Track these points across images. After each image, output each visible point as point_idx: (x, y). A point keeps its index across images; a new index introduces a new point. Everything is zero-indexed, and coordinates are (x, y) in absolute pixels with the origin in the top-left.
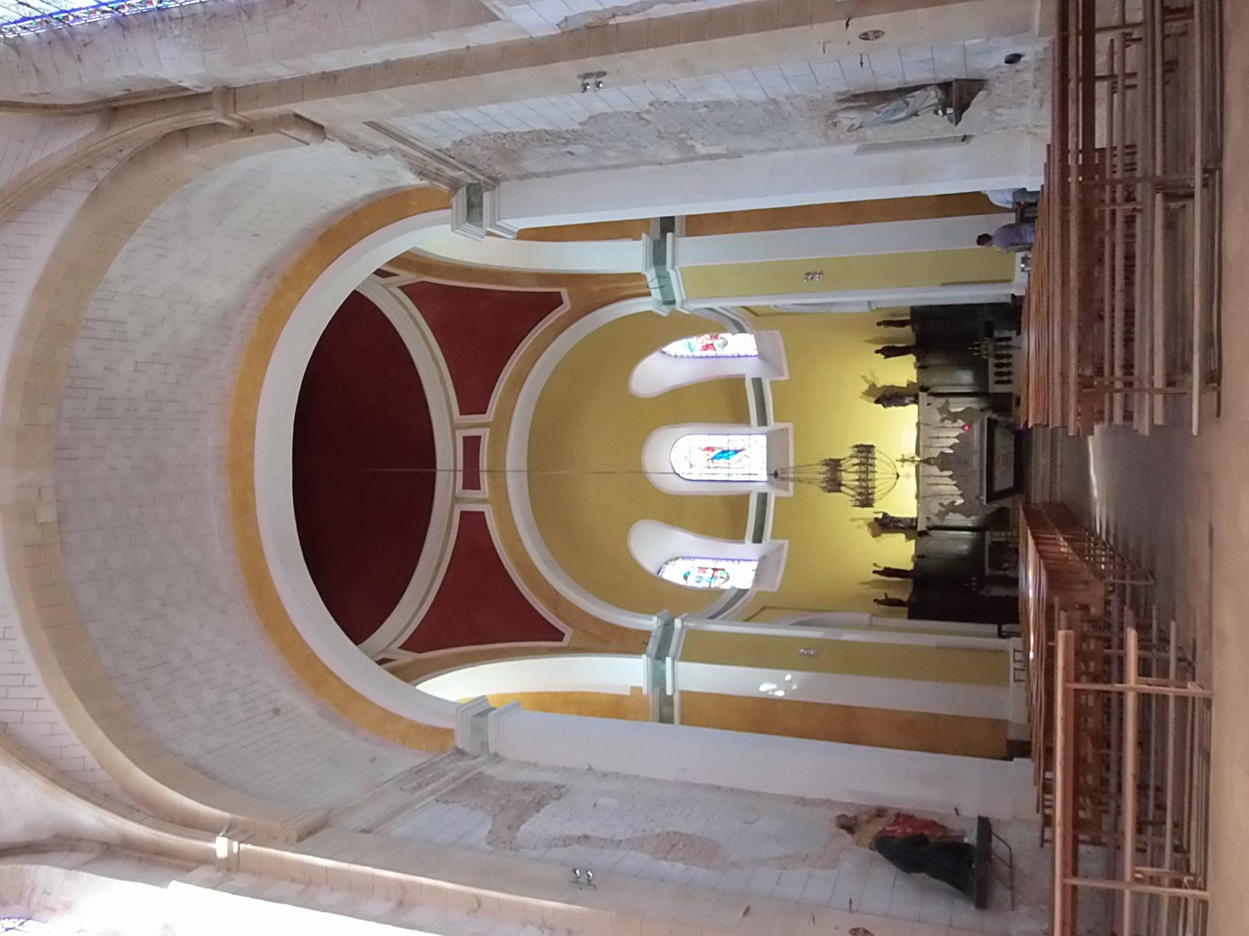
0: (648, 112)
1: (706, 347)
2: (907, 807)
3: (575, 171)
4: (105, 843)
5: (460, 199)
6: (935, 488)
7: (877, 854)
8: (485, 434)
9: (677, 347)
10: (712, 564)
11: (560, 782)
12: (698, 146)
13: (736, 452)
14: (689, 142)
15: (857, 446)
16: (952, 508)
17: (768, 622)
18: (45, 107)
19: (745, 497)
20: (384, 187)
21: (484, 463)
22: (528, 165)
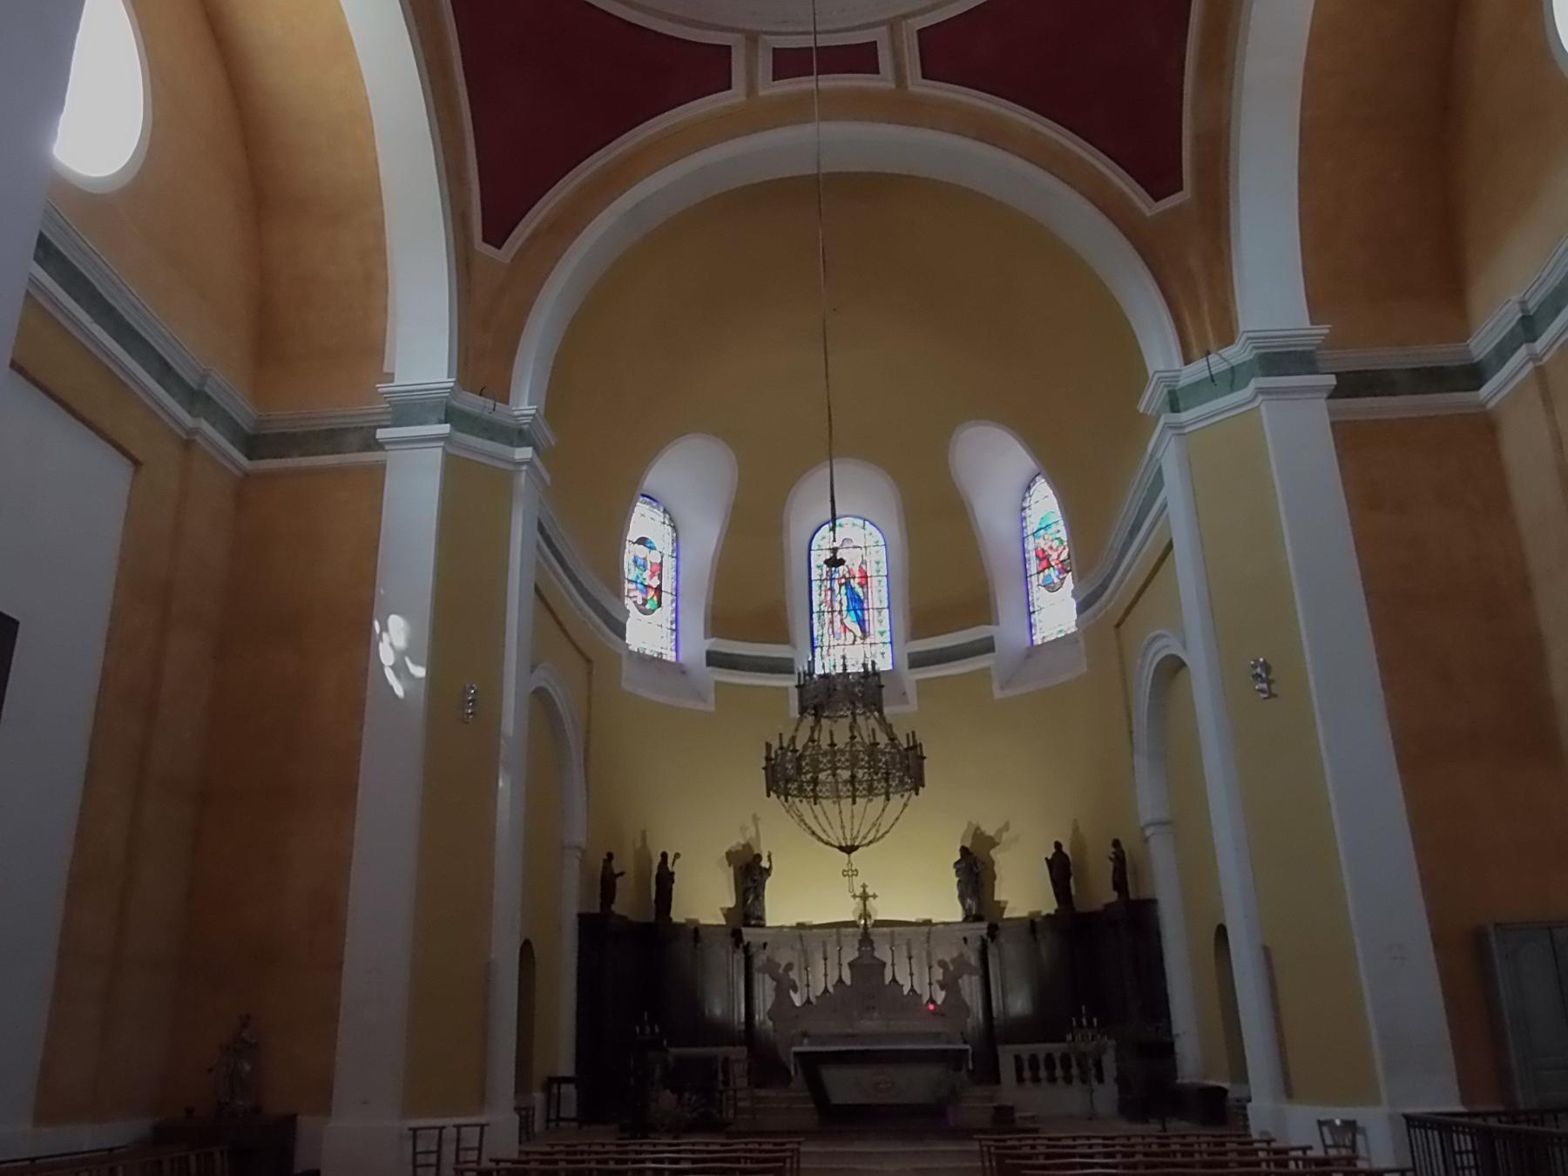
1: (1043, 557)
6: (819, 956)
8: (884, 81)
9: (1044, 504)
10: (668, 586)
16: (784, 987)
19: (783, 637)
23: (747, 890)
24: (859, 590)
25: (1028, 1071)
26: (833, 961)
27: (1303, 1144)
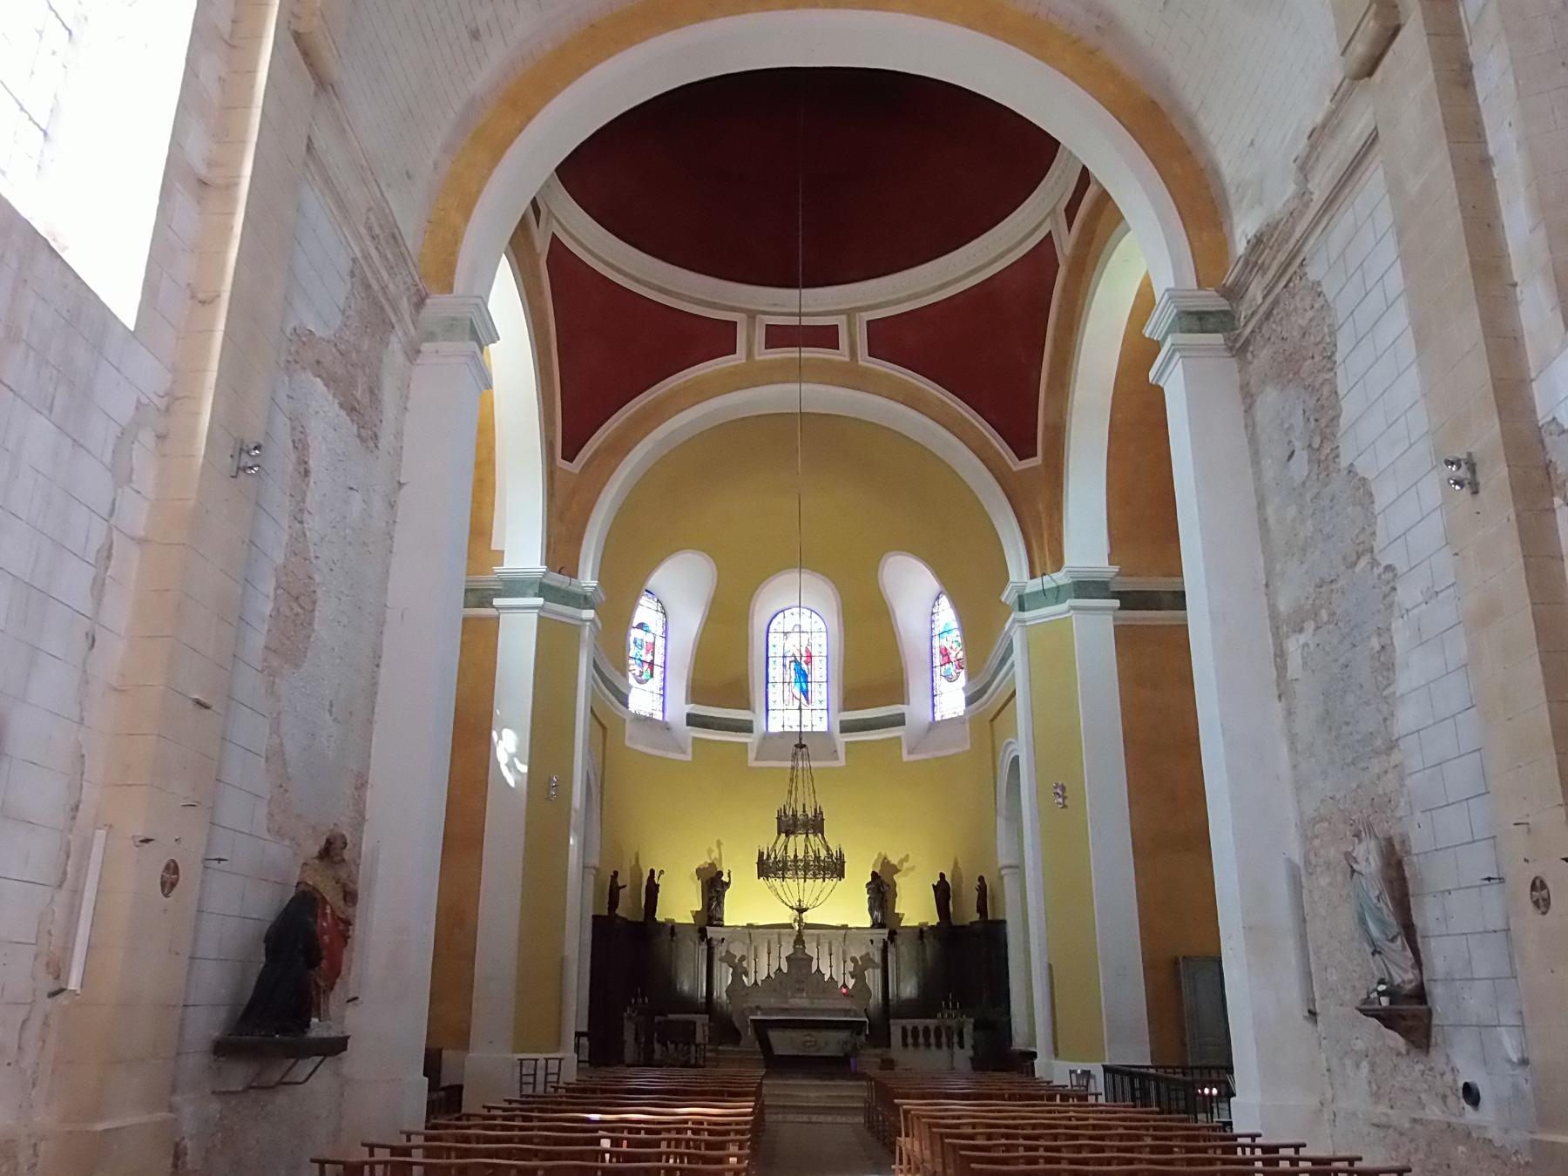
0: (1374, 563)
1: (945, 653)
2: (357, 931)
3: (1256, 461)
5: (1211, 301)
7: (292, 893)
8: (841, 355)
9: (946, 615)
10: (659, 660)
11: (382, 443)
12: (1302, 638)
13: (805, 693)
16: (739, 972)
17: (590, 739)
19: (746, 705)
20: (1232, 190)
21: (810, 353)
22: (1270, 398)
23: (711, 899)
24: (804, 666)
25: (913, 1038)
26: (774, 954)
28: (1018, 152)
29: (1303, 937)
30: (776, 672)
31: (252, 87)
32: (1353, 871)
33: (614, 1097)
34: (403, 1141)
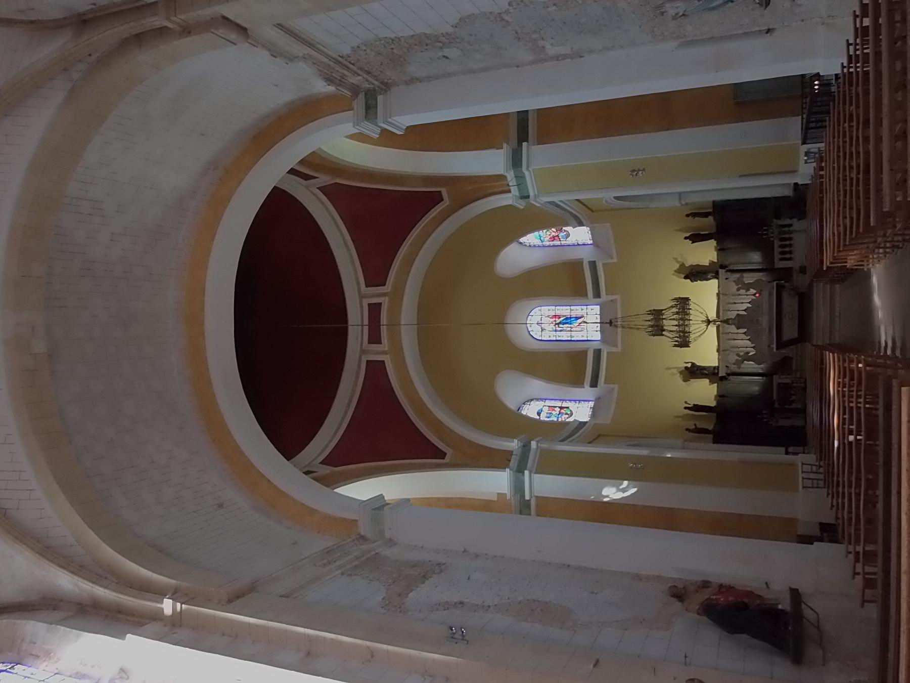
0: (507, 12)
4: (80, 604)
7: (705, 618)
8: (385, 302)
9: (531, 239)
10: (559, 404)
12: (548, 47)
13: (577, 318)
14: (541, 43)
15: (675, 299)
16: (747, 357)
18: (32, 22)
19: (584, 353)
21: (384, 319)
22: (414, 69)
25: (786, 254)
26: (735, 336)
27: (851, 18)
28: (279, 210)
29: (722, 38)
30: (565, 336)
31: (257, 626)
32: (684, 15)
33: (825, 431)
34: (851, 556)
